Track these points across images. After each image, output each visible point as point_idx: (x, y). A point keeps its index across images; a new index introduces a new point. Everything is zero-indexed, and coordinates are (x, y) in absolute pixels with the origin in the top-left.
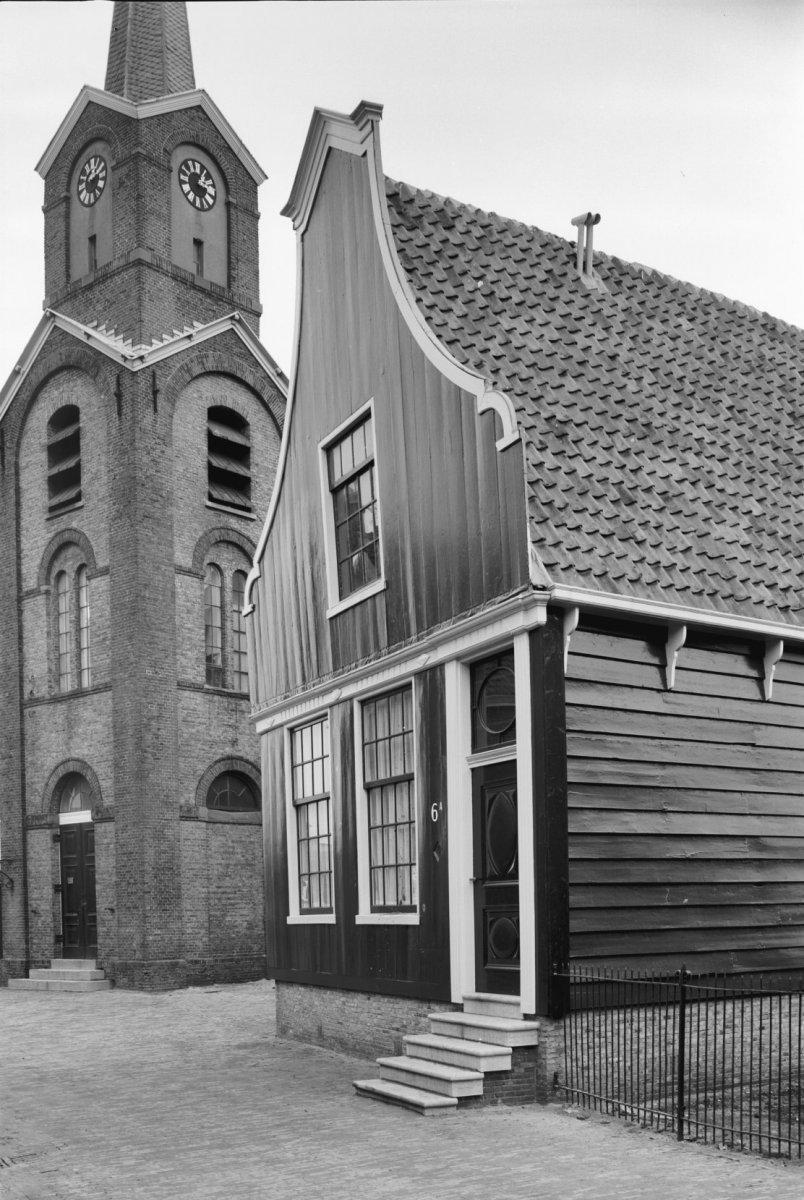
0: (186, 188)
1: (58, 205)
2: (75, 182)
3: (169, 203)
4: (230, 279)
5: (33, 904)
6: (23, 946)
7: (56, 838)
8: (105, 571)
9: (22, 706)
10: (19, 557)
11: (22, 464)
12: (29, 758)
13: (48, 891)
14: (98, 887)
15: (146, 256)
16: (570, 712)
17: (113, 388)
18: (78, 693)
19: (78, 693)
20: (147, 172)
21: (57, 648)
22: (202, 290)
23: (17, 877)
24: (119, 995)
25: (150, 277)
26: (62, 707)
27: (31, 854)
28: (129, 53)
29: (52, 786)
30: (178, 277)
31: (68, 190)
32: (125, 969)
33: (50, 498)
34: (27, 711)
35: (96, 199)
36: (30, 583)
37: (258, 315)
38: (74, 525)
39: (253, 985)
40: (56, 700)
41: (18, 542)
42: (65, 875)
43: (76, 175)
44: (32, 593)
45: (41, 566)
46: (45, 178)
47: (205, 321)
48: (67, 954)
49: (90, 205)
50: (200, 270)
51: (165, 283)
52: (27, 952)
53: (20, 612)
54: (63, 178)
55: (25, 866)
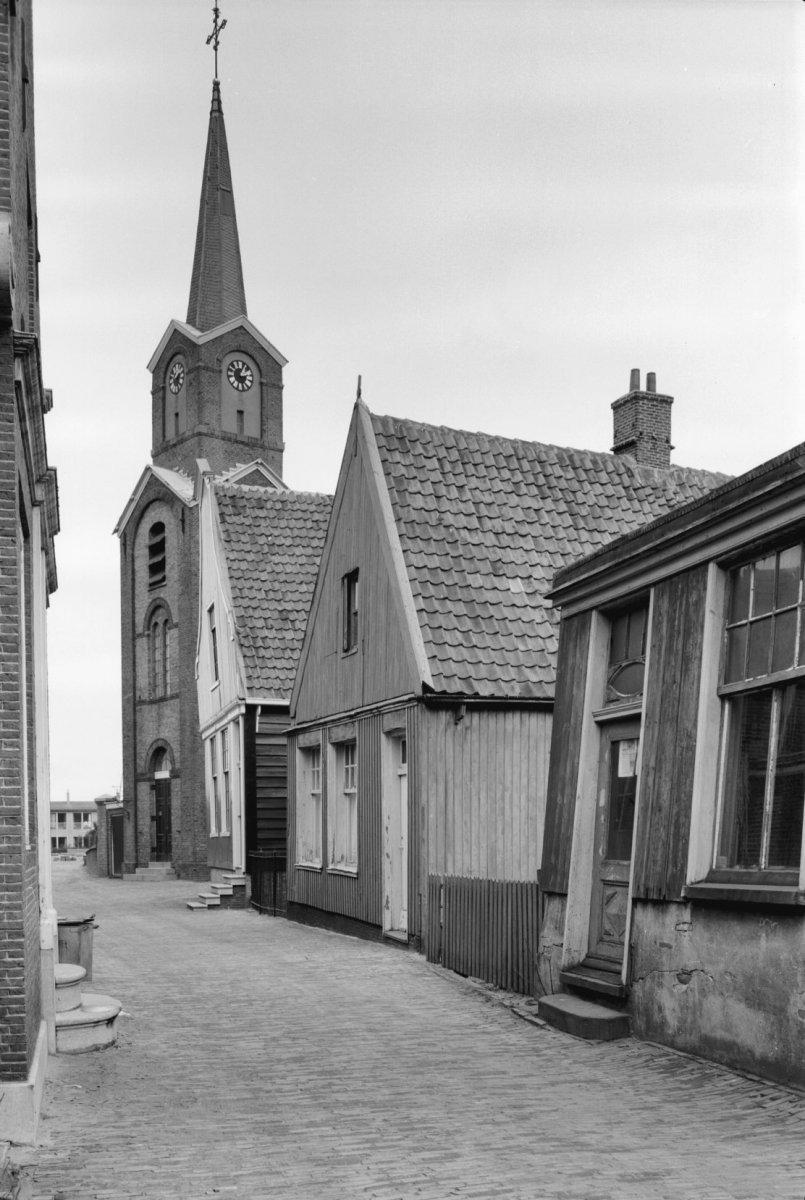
0: (232, 379)
1: (159, 392)
2: (168, 377)
3: (220, 392)
4: (262, 431)
5: (140, 828)
6: (134, 854)
7: (153, 788)
8: (176, 626)
9: (135, 705)
10: (134, 612)
11: (136, 555)
12: (139, 738)
13: (148, 820)
14: (173, 818)
15: (203, 429)
16: (257, 748)
17: (180, 517)
18: (163, 699)
19: (163, 699)
20: (205, 377)
21: (154, 669)
22: (242, 443)
23: (131, 811)
24: (180, 882)
25: (206, 441)
26: (155, 707)
27: (139, 797)
28: (200, 295)
29: (150, 755)
30: (226, 438)
31: (164, 382)
32: (184, 867)
33: (150, 577)
34: (138, 708)
35: (179, 390)
36: (140, 629)
37: (282, 451)
38: (162, 595)
39: (707, 927)
40: (152, 702)
41: (133, 603)
42: (158, 811)
43: (169, 373)
44: (141, 635)
45: (145, 619)
46: (153, 372)
47: (245, 462)
48: (158, 859)
49: (176, 394)
50: (241, 429)
51: (217, 443)
52: (137, 858)
53: (134, 646)
54: (162, 374)
55: (136, 806)
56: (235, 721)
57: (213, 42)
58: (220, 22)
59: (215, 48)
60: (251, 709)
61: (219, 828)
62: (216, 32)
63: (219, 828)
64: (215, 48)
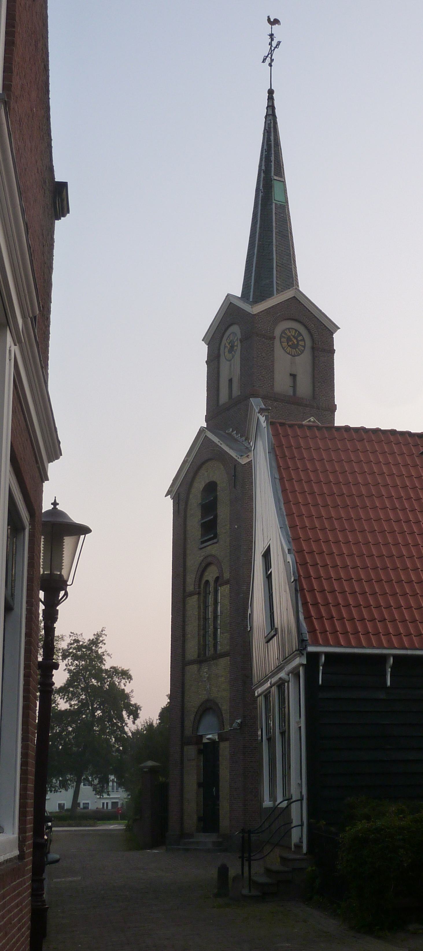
8: (227, 582)
35: (233, 357)
36: (190, 588)
44: (191, 594)
46: (208, 345)
56: (295, 673)
57: (268, 60)
58: (274, 44)
59: (270, 65)
60: (313, 658)
61: (273, 797)
62: (271, 52)
63: (273, 797)
64: (270, 65)
